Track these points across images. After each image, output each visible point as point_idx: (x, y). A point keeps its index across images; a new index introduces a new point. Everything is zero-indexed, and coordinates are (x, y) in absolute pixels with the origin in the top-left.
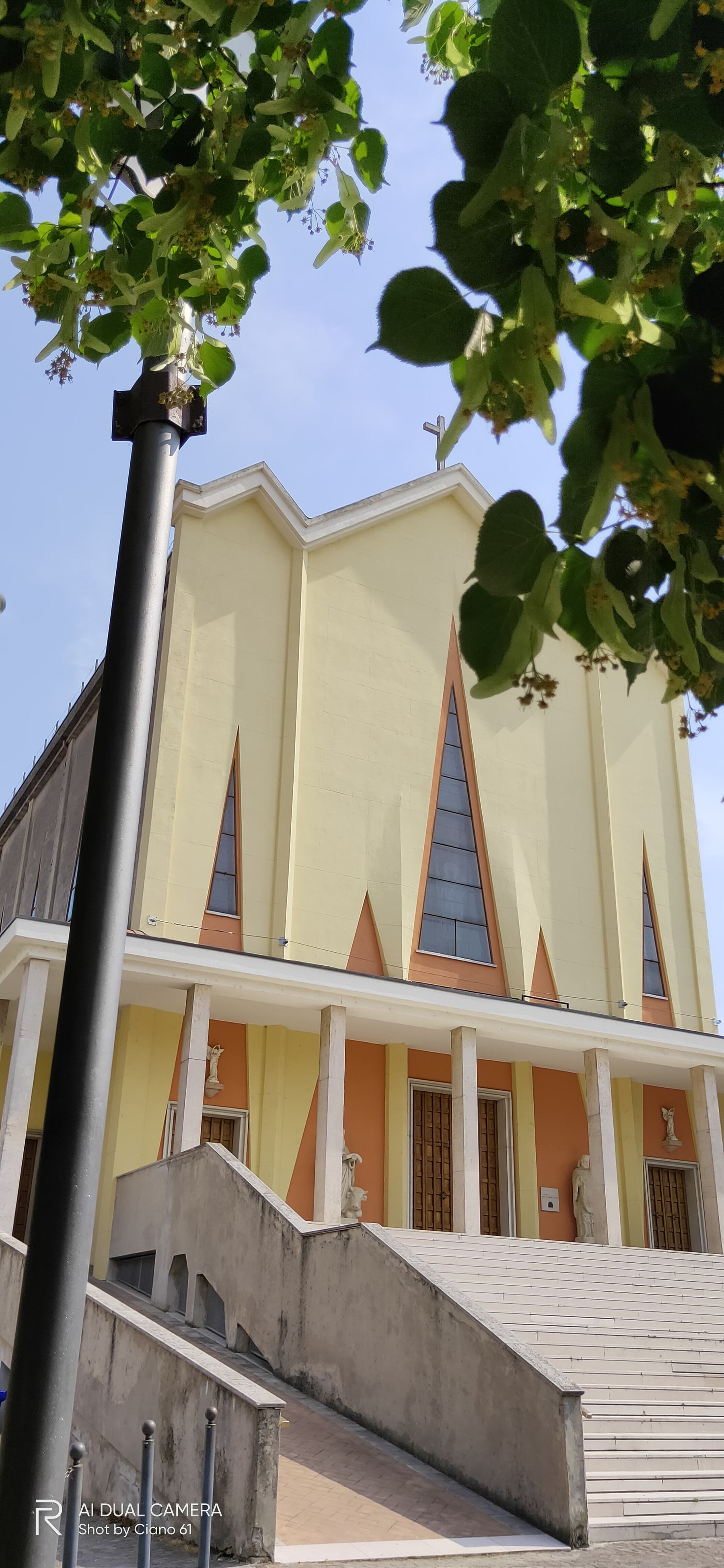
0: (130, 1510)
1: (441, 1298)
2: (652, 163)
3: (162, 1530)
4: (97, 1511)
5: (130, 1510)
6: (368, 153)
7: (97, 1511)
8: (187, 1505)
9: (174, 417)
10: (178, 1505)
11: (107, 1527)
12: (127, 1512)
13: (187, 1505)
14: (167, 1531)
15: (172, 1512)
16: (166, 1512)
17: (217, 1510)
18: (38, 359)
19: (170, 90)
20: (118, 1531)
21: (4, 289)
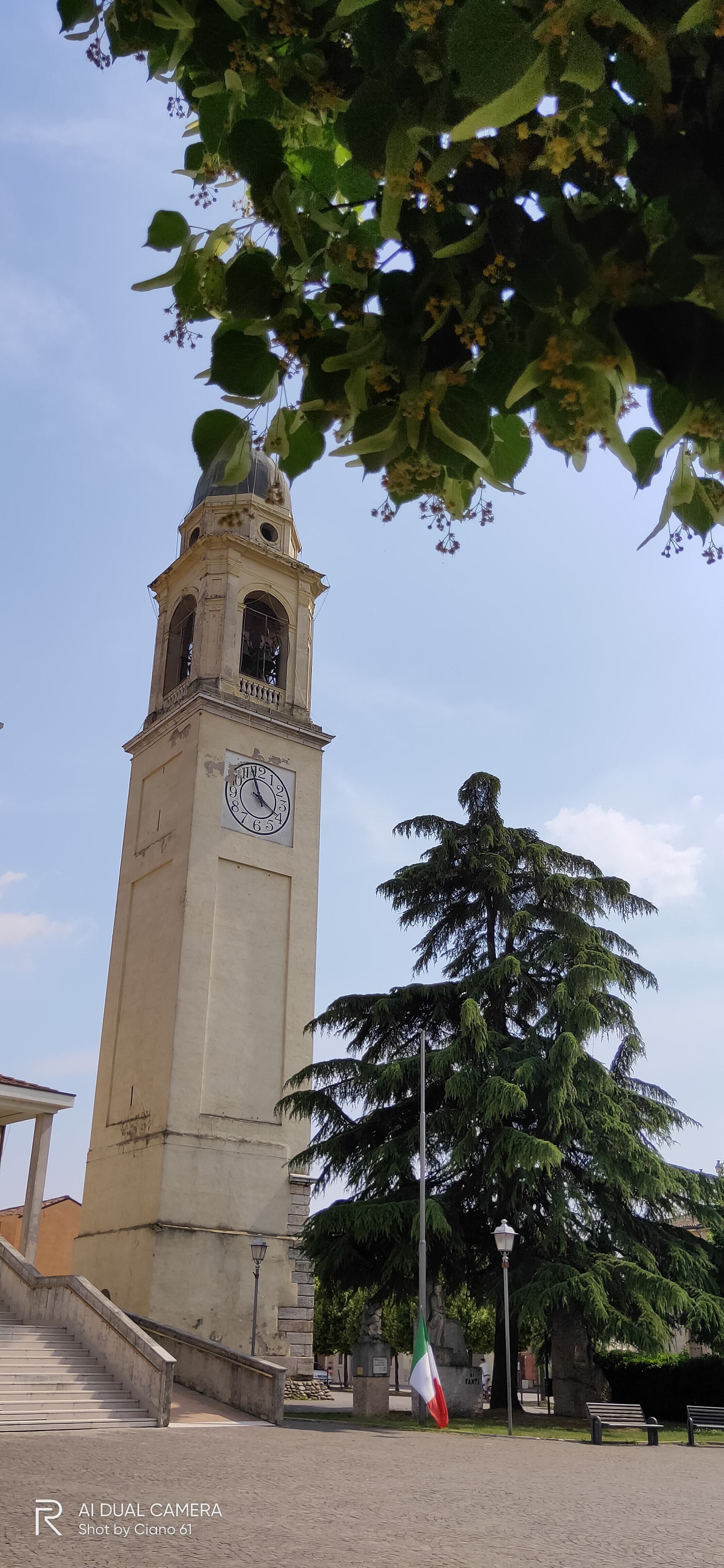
0: (130, 1510)
1: (412, 487)
2: (454, 168)
3: (162, 1530)
4: (97, 1512)
5: (130, 1510)
6: (353, 153)
7: (97, 1512)
8: (187, 1505)
9: (428, 74)
10: (178, 1505)
11: (107, 1527)
12: (127, 1512)
13: (187, 1505)
14: (167, 1531)
15: (172, 1512)
16: (166, 1512)
17: (217, 1510)
18: (197, 377)
19: (625, 149)
20: (118, 1530)
21: (166, 338)
